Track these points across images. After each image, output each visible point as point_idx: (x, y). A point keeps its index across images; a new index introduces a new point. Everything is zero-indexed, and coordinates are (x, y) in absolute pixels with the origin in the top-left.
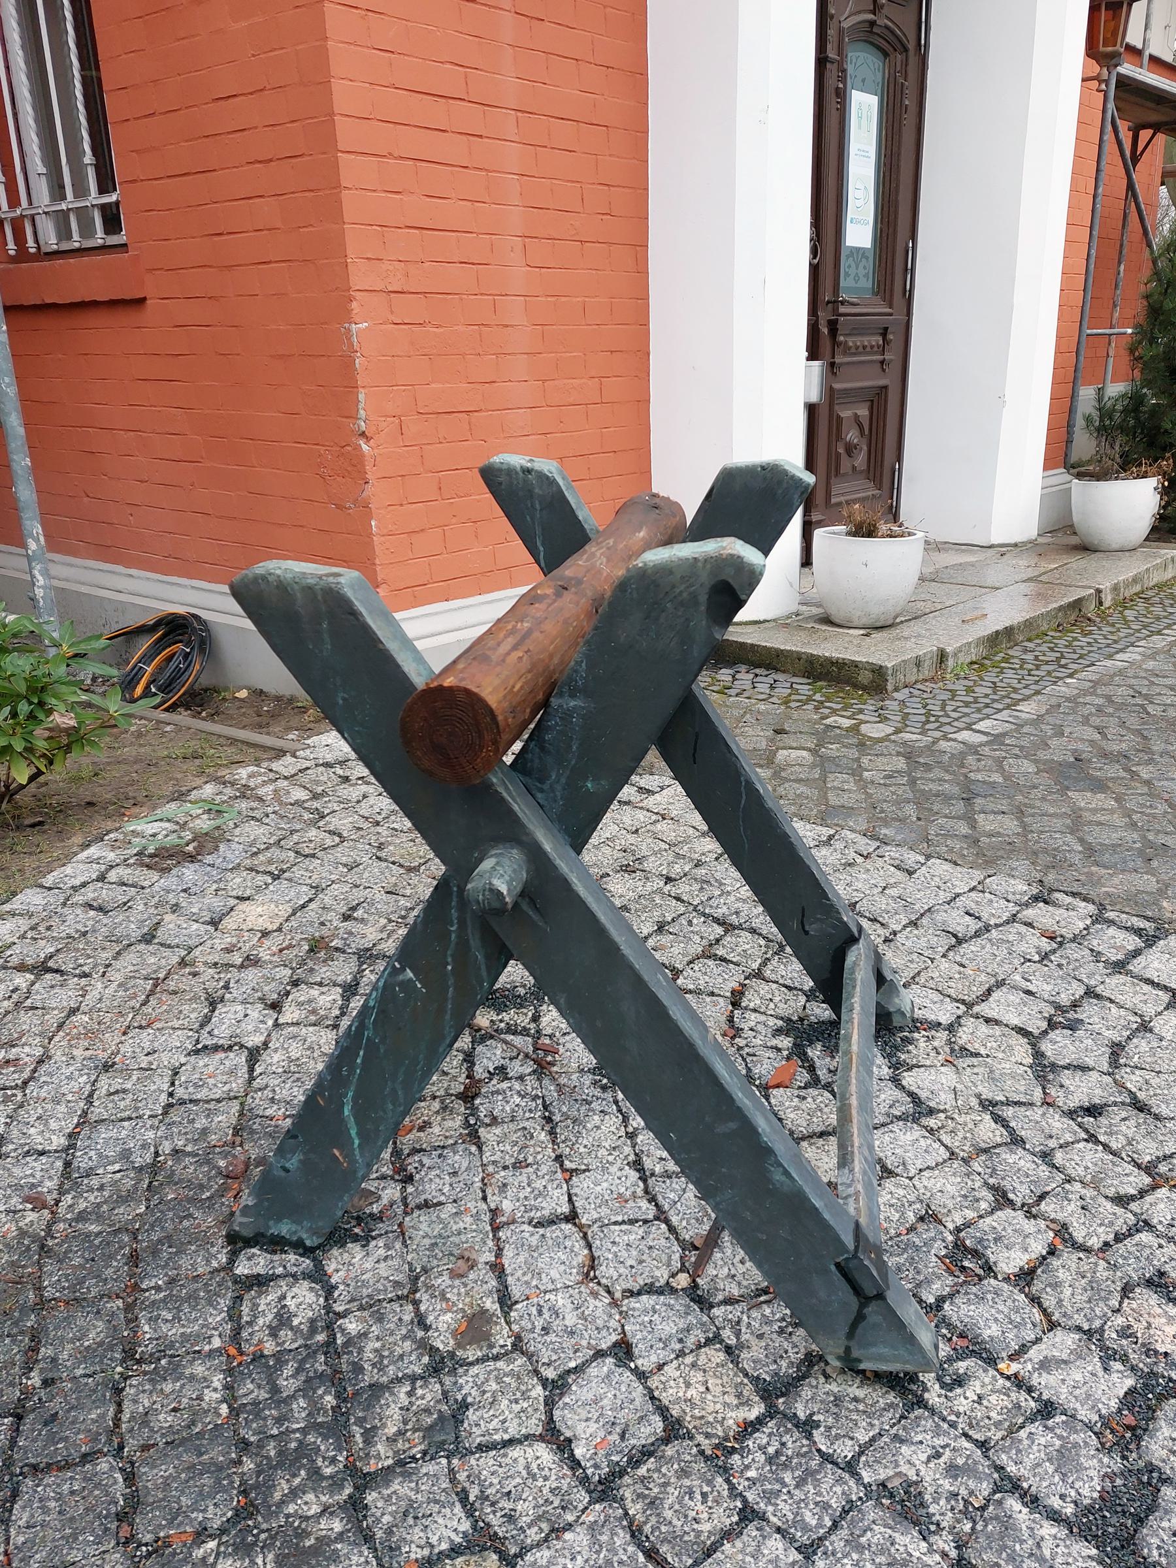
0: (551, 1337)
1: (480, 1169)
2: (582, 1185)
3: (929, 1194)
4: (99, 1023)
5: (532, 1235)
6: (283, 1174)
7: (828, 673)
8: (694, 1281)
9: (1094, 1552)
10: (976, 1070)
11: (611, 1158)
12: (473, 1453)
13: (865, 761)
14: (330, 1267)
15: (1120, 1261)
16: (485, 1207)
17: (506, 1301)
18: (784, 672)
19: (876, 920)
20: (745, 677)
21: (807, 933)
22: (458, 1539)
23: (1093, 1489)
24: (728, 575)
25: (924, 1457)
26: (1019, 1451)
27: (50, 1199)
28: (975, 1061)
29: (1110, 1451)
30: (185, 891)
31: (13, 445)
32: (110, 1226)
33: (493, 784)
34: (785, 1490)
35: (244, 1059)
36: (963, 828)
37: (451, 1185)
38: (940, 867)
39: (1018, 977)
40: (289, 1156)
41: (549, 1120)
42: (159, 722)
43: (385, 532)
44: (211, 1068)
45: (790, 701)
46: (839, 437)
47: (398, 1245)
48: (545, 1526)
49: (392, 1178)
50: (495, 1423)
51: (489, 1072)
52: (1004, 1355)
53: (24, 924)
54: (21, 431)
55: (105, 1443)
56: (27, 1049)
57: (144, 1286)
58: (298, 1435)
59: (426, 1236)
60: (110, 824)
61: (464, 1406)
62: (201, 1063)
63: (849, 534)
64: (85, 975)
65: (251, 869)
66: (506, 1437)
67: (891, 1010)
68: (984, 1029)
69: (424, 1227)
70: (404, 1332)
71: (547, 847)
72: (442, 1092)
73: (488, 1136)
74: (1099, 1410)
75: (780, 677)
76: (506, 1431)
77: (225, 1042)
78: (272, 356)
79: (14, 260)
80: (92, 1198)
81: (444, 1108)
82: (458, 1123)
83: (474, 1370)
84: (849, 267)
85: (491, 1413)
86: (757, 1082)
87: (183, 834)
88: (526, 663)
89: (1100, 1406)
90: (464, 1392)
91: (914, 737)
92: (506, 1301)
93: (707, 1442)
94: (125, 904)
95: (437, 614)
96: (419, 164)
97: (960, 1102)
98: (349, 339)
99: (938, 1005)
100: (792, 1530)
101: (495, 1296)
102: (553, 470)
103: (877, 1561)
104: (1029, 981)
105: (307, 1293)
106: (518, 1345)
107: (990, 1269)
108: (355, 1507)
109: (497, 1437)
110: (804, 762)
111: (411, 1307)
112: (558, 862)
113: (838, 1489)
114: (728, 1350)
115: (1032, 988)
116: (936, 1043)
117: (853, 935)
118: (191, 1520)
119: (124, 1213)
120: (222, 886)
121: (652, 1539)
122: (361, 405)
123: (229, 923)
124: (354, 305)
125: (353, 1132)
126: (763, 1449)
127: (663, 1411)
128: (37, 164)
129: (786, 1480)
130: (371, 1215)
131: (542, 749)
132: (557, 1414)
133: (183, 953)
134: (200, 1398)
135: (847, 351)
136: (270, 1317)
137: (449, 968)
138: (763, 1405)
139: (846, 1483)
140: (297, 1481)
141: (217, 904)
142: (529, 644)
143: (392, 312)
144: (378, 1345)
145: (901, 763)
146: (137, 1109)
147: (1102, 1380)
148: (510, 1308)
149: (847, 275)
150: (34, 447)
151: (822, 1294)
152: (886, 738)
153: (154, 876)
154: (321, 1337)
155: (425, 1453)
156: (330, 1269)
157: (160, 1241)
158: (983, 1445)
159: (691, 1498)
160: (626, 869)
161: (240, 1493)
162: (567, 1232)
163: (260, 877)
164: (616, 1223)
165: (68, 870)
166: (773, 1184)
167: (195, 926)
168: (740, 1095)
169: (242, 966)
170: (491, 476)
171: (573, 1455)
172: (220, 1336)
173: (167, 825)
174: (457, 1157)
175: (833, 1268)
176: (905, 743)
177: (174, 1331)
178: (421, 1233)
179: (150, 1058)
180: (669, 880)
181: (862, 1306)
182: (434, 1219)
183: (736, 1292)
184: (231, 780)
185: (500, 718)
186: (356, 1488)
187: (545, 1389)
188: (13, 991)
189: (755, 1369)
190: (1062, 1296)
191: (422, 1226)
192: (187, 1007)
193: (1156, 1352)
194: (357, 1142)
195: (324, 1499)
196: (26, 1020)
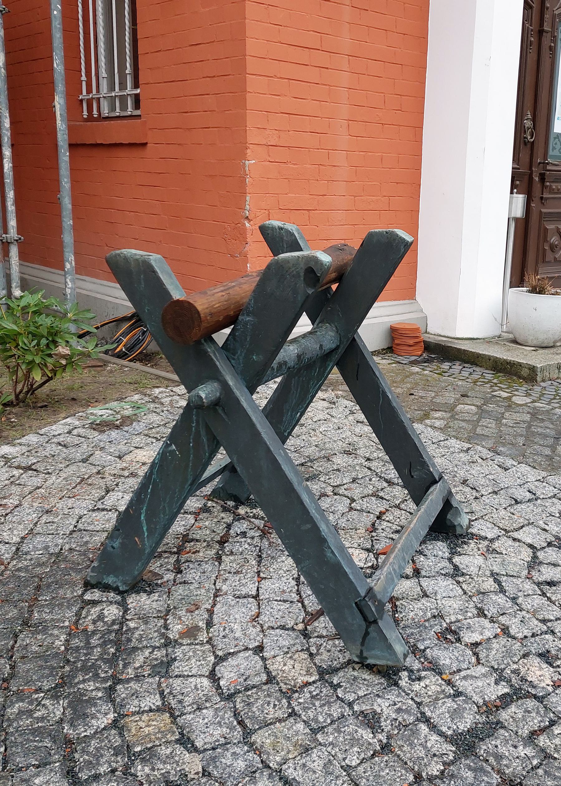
0: (227, 640)
1: (217, 572)
2: (265, 584)
3: (443, 607)
4: (49, 494)
5: (233, 600)
6: (112, 550)
7: (505, 368)
8: (306, 628)
9: (454, 749)
10: (496, 559)
11: (284, 575)
12: (172, 678)
13: (507, 414)
14: (129, 600)
15: (529, 644)
16: (214, 587)
17: (209, 624)
18: (481, 367)
19: (475, 489)
20: (457, 367)
21: (412, 477)
22: (153, 707)
23: (465, 727)
24: (312, 264)
25: (387, 705)
26: (435, 707)
27: (6, 562)
28: (497, 556)
29: (482, 713)
30: (110, 442)
31: (64, 213)
32: (31, 574)
33: (208, 352)
34: (314, 708)
35: (116, 516)
36: (548, 452)
37: (200, 577)
38: (524, 468)
39: (541, 522)
40: (115, 540)
41: (260, 556)
42: (122, 366)
44: (98, 518)
45: (477, 382)
46: (545, 240)
47: (165, 597)
48: (195, 707)
49: (172, 571)
50: (186, 668)
51: (237, 534)
52: (447, 671)
53: (24, 449)
54: (70, 206)
55: (5, 653)
56: (11, 501)
57: (40, 599)
58: (93, 661)
59: (181, 595)
60: (81, 409)
61: (175, 659)
62: (94, 515)
63: (530, 292)
64: (49, 473)
65: (146, 435)
67: (456, 524)
68: (510, 542)
69: (180, 591)
70: (156, 629)
71: (231, 383)
72: (209, 539)
73: (226, 559)
74: (484, 698)
75: (478, 369)
77: (109, 508)
78: (206, 176)
79: (86, 120)
80: (26, 563)
81: (208, 546)
82: (213, 552)
83: (185, 647)
84: (556, 144)
85: (186, 664)
86: (375, 551)
87: (116, 416)
88: (226, 297)
89: (485, 696)
90: (176, 655)
91: (541, 405)
92: (209, 624)
93: (285, 686)
94: (78, 445)
96: (291, 81)
97: (480, 572)
98: (244, 168)
99: (489, 530)
100: (311, 722)
101: (205, 622)
102: (293, 229)
103: (346, 737)
104: (547, 525)
105: (115, 610)
106: (210, 641)
107: (459, 640)
108: (111, 689)
109: (186, 673)
110: (471, 412)
111: (163, 621)
112: (235, 390)
113: (339, 710)
114: (311, 655)
115: (547, 528)
116: (480, 546)
117: (435, 479)
118: (35, 685)
119: (38, 570)
120: (129, 441)
121: (243, 717)
122: (247, 203)
123: (127, 458)
124: (248, 151)
125: (145, 529)
126: (310, 692)
127: (268, 673)
128: (103, 73)
129: (316, 704)
130: (157, 584)
131: (234, 339)
132: (217, 668)
133: (100, 468)
134: (53, 643)
135: (551, 191)
136: (95, 616)
137: (191, 445)
138: (318, 677)
139: (344, 708)
140: (87, 677)
141: (124, 448)
142: (231, 291)
143: (269, 156)
144: (142, 633)
145: (527, 417)
146: (57, 530)
147: (492, 687)
148: (211, 627)
149: (554, 148)
150: (76, 217)
151: (350, 620)
152: (526, 405)
153: (96, 433)
154: (116, 627)
155: (149, 675)
156: (129, 602)
157: (52, 582)
158: (419, 704)
159: (268, 705)
160: (348, 453)
161: (60, 678)
162: (250, 602)
163: (150, 439)
164: (276, 600)
165: (54, 427)
166: (327, 558)
167: (110, 457)
168: (314, 511)
169: (128, 477)
170: (263, 230)
171: (219, 684)
172: (69, 621)
173: (110, 412)
174: (207, 566)
175: (354, 605)
176: (535, 408)
177: (48, 617)
178: (178, 593)
179: (70, 510)
180: (368, 459)
181: (368, 627)
182: (186, 588)
183: (324, 634)
184: (150, 394)
185: (202, 315)
186: (114, 683)
187: (215, 659)
188: (11, 477)
189: (320, 663)
190: (490, 654)
191: (180, 590)
192: (95, 491)
193: (526, 680)
194: (146, 534)
195: (97, 685)
196: (14, 489)
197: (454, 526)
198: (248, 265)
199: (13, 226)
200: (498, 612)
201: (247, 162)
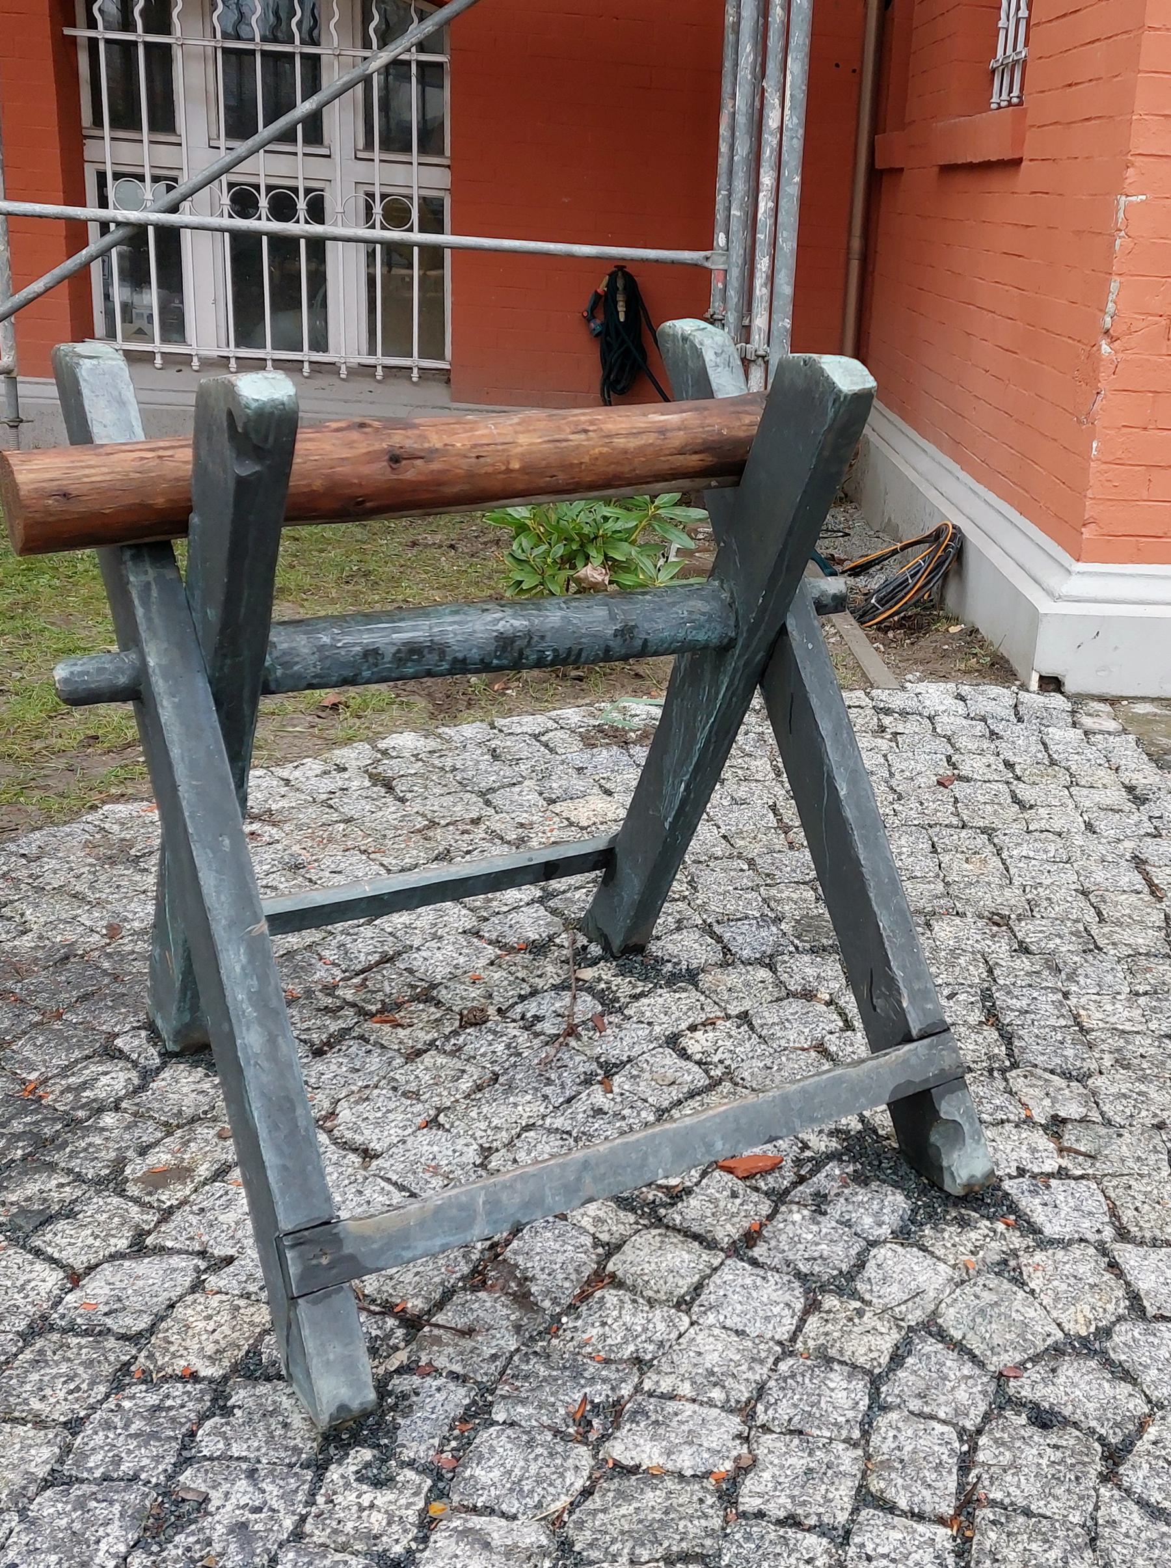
43: (1111, 458)
66: (56, 1255)
76: (60, 1251)
85: (72, 1232)
95: (1131, 575)
109: (50, 1250)
122: (1112, 297)
197: (941, 1168)
198: (1095, 445)
199: (760, 329)
200: (790, 1420)
201: (1123, 198)
